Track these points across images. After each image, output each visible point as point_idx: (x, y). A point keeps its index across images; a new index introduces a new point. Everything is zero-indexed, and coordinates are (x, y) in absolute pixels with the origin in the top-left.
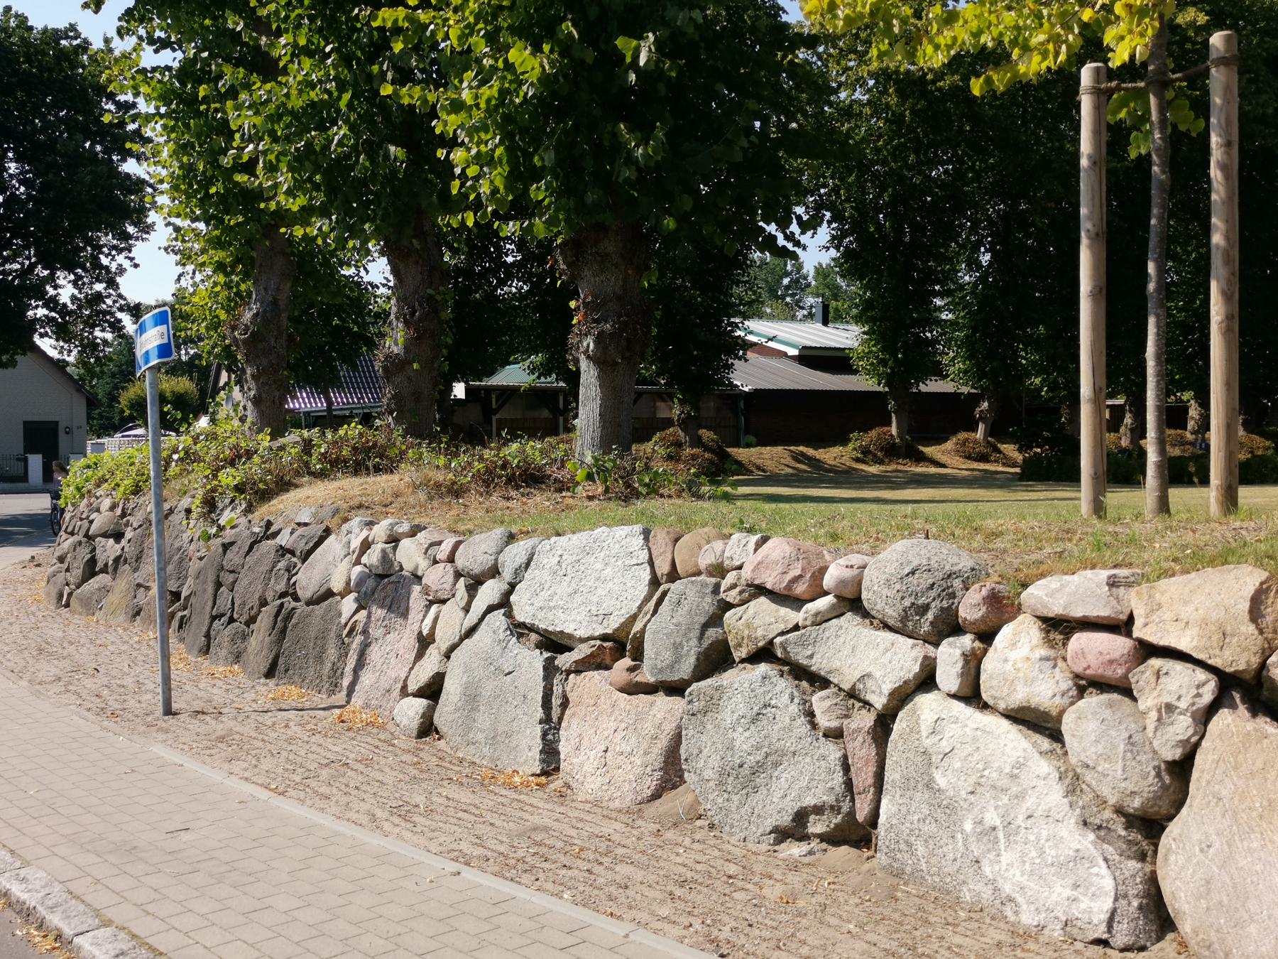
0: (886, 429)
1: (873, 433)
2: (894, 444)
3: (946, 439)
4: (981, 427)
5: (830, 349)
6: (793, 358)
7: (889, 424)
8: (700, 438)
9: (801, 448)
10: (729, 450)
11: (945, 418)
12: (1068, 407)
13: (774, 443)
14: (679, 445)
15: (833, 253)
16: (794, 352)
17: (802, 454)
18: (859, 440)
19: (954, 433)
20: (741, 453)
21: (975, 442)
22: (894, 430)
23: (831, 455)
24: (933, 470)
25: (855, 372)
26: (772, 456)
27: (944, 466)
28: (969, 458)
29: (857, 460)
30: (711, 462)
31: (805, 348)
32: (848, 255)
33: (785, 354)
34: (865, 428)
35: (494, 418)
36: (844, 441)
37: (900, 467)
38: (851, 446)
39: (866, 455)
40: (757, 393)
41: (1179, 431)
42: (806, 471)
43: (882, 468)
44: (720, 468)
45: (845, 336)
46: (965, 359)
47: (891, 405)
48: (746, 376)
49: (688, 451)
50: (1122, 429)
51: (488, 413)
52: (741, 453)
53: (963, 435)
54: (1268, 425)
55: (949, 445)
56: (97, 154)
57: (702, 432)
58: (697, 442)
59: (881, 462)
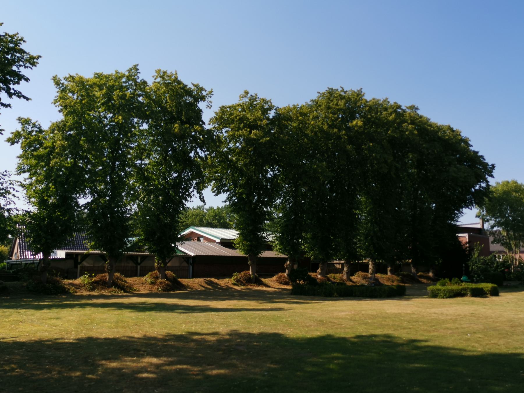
0: (247, 272)
1: (243, 273)
2: (250, 278)
3: (273, 276)
4: (287, 271)
5: (225, 239)
6: (218, 243)
7: (249, 270)
8: (166, 275)
9: (213, 279)
10: (179, 280)
11: (272, 267)
12: (322, 264)
13: (200, 277)
14: (157, 278)
15: (228, 203)
16: (218, 241)
17: (211, 281)
18: (237, 275)
19: (277, 273)
20: (185, 281)
21: (284, 277)
22: (250, 272)
23: (223, 282)
24: (264, 288)
25: (236, 249)
26: (196, 283)
27: (269, 287)
28: (281, 283)
29: (234, 284)
30: (168, 285)
31: (222, 239)
32: (233, 205)
33: (215, 241)
34: (240, 272)
35: (79, 266)
36: (230, 276)
37: (252, 287)
38: (233, 278)
39: (238, 282)
40: (197, 257)
41: (366, 273)
42: (210, 289)
43: (243, 287)
44: (173, 287)
45: (231, 234)
46: (280, 245)
47: (249, 262)
48: (187, 249)
49: (159, 280)
50: (344, 272)
51: (76, 264)
52: (185, 281)
53: (280, 274)
54: (401, 271)
55: (275, 278)
56: (474, 187)
57: (167, 272)
58: (165, 276)
59: (244, 285)
